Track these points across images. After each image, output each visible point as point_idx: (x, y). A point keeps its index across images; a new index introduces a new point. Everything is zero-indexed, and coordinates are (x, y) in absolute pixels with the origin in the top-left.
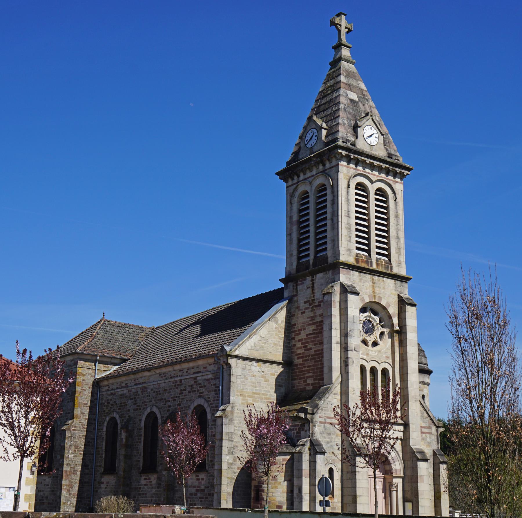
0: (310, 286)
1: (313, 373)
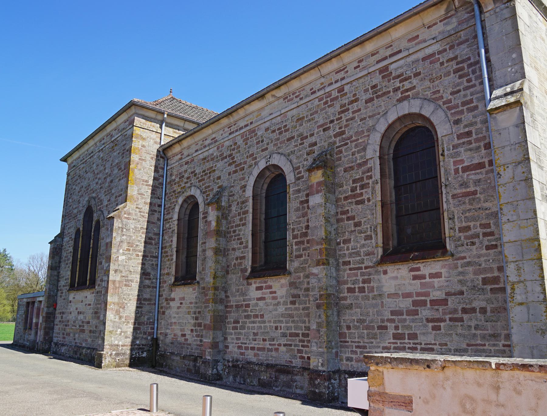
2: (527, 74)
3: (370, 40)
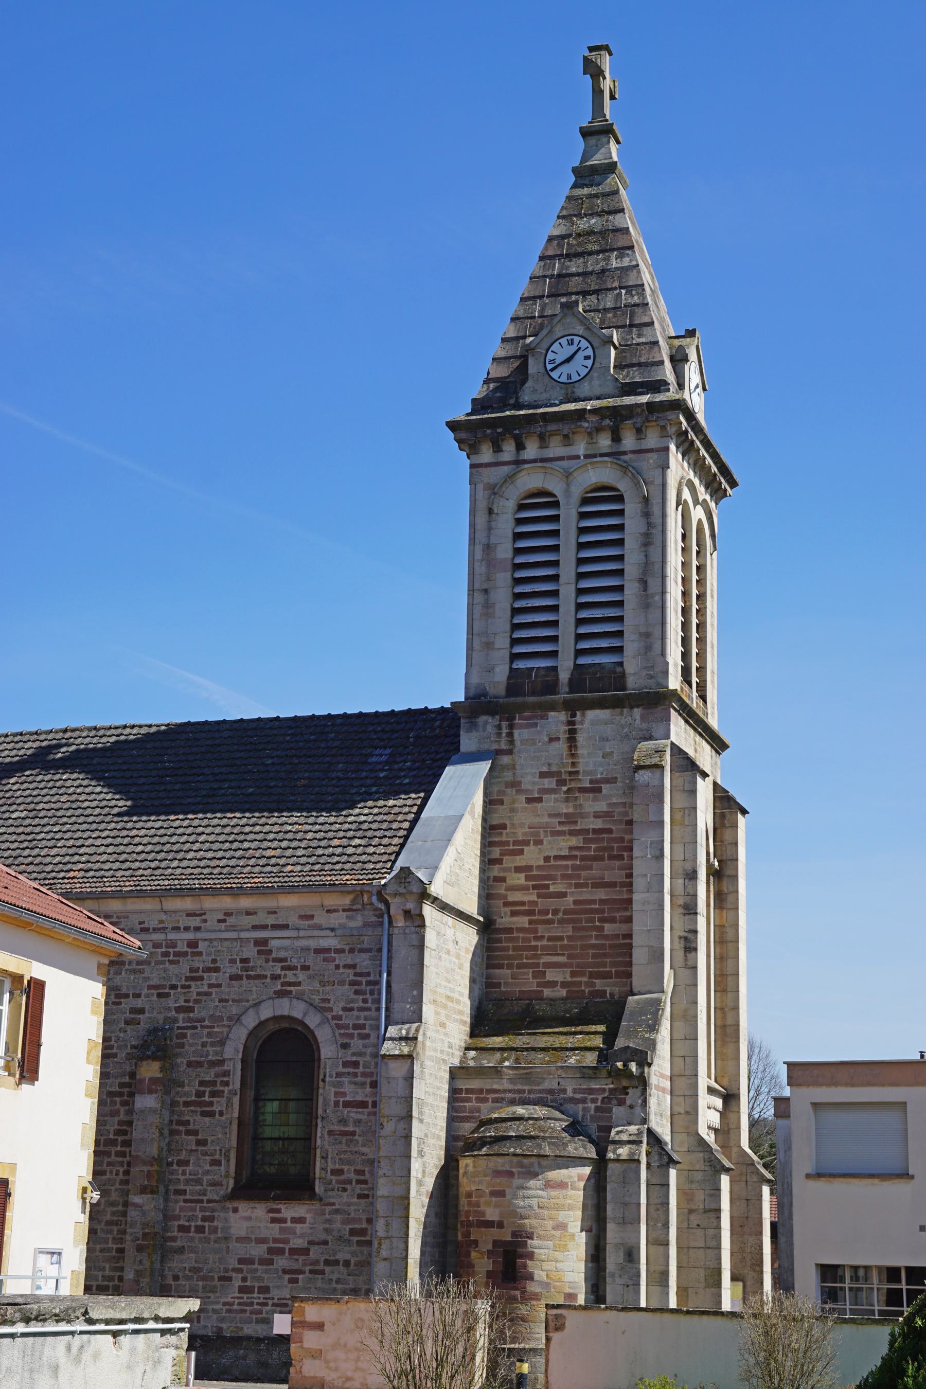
0: (563, 736)
1: (570, 957)
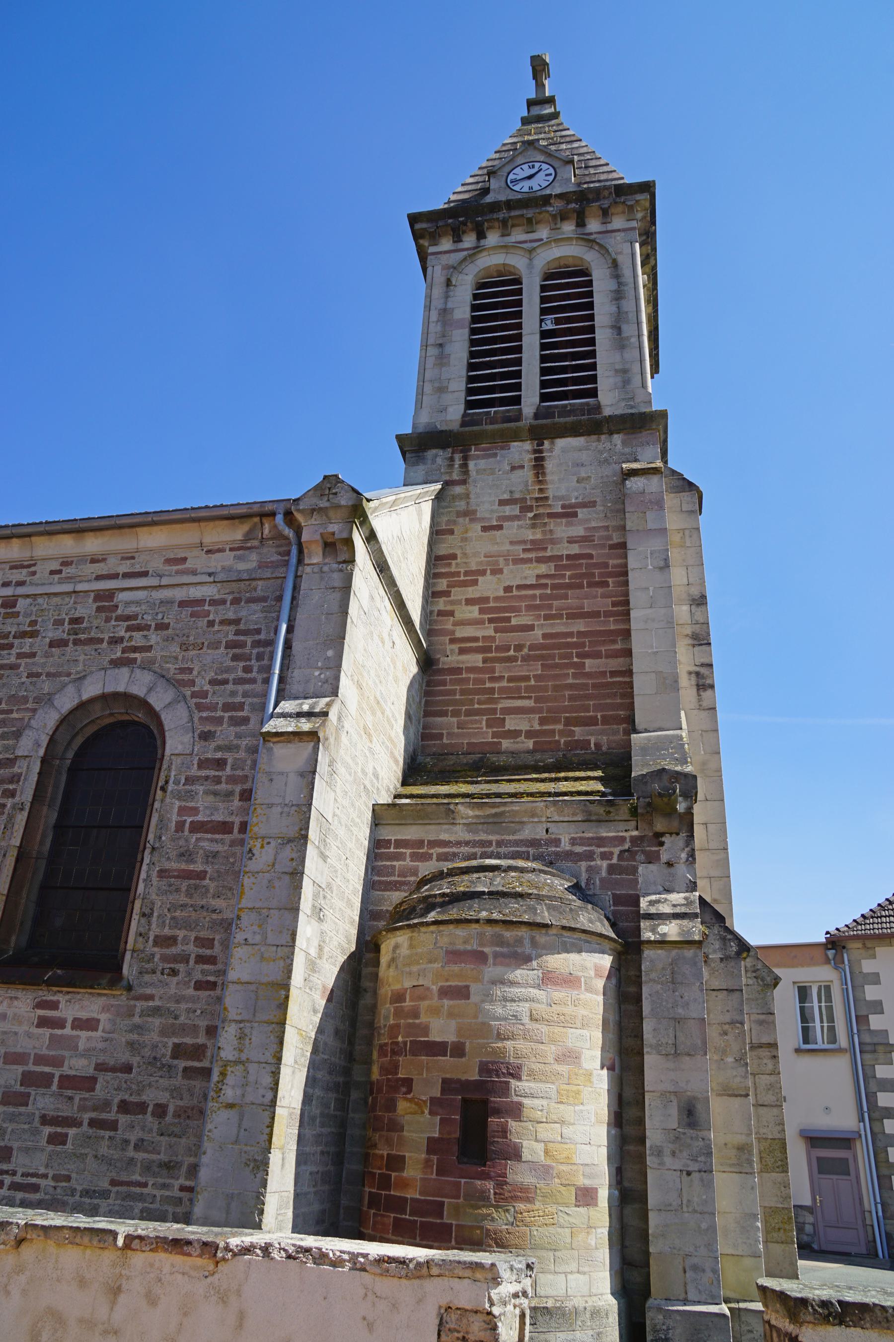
1: (537, 700)
2: (341, 691)
3: (98, 533)
